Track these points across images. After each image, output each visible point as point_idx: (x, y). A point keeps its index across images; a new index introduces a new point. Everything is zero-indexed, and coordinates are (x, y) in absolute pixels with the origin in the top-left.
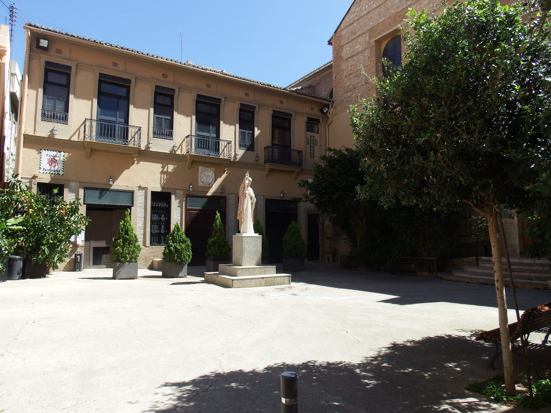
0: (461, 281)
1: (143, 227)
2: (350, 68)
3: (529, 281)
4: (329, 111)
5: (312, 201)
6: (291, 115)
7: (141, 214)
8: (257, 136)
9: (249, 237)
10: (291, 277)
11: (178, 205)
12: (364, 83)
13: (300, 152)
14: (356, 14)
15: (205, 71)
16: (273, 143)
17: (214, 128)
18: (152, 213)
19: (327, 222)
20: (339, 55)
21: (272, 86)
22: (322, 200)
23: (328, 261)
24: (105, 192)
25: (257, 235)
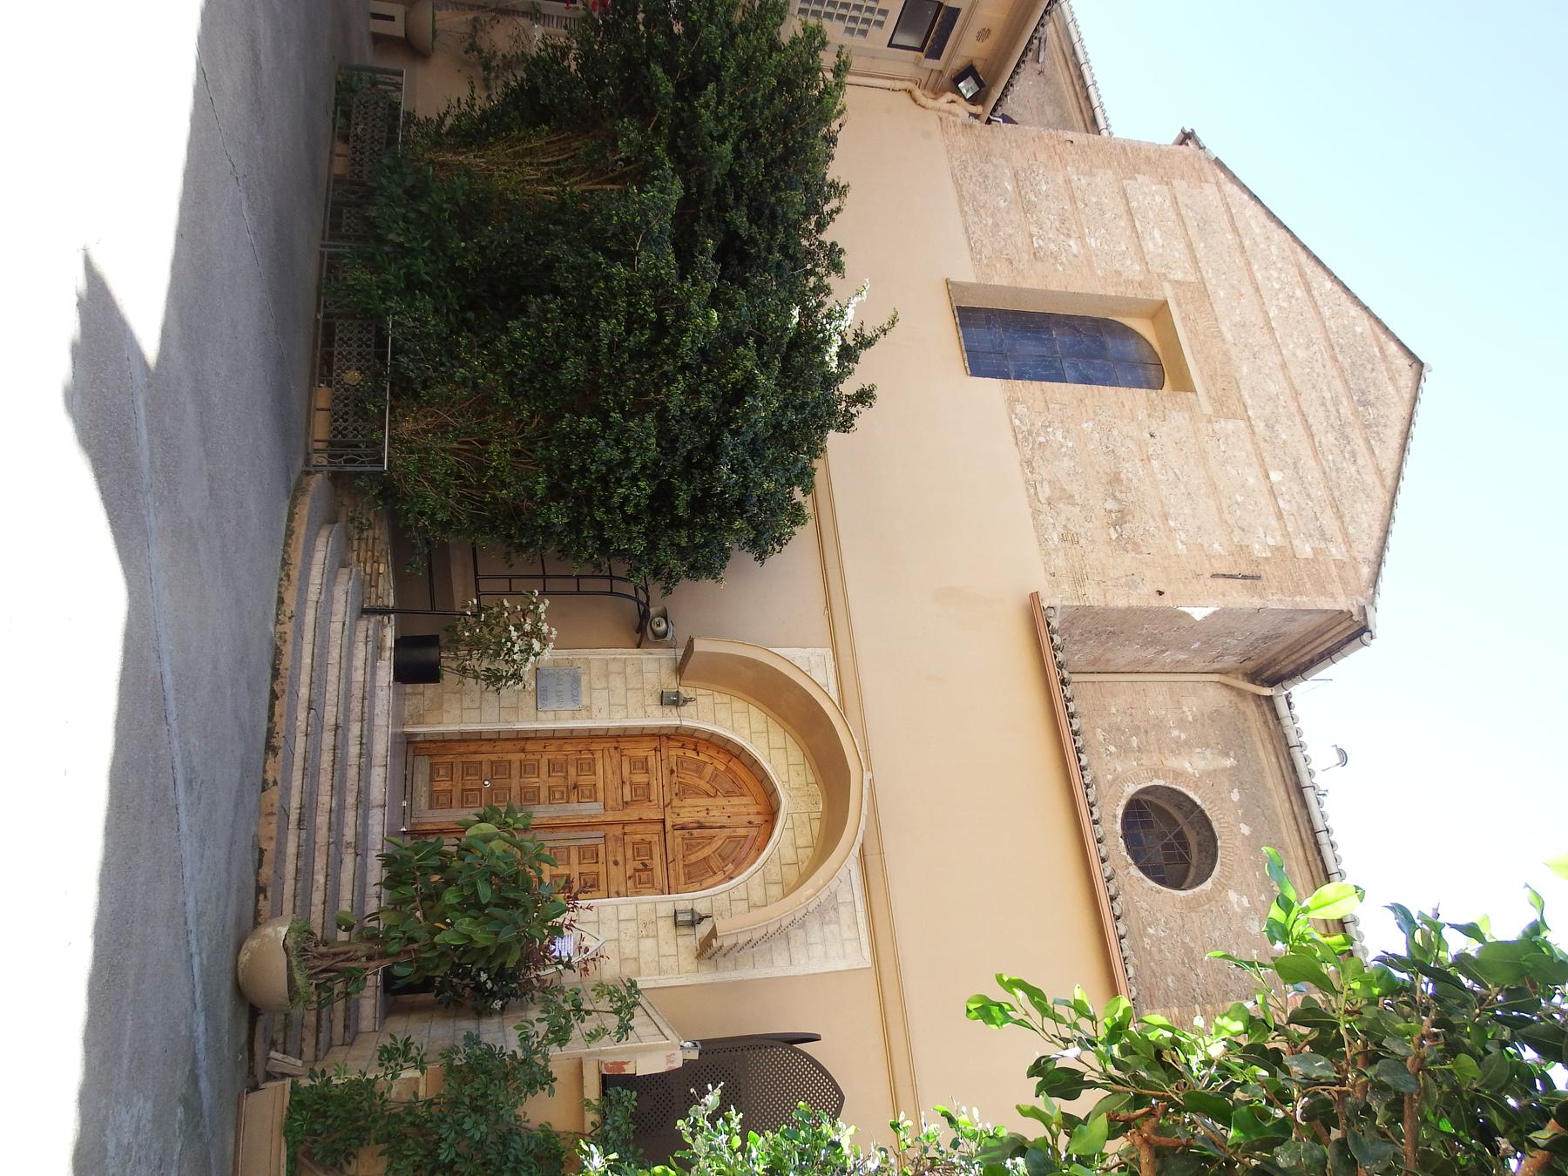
0: (288, 575)
2: (1094, 200)
3: (294, 817)
12: (1036, 245)
14: (1262, 246)
19: (538, 31)
20: (1143, 167)
22: (641, 16)
23: (376, 16)
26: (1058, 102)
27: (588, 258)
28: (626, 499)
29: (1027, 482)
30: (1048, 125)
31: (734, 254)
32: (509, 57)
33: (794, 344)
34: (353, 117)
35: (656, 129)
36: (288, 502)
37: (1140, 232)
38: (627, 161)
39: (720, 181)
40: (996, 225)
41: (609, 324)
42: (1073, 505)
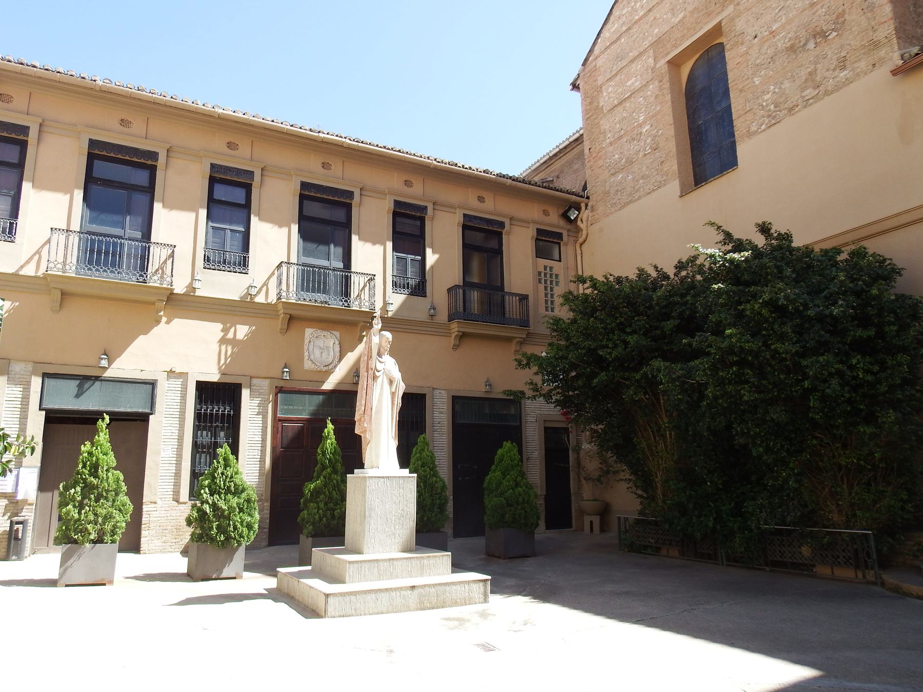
1: (175, 459)
2: (618, 125)
4: (580, 216)
5: (548, 396)
6: (502, 225)
7: (170, 431)
8: (432, 267)
9: (383, 477)
10: (489, 583)
11: (257, 411)
12: (650, 151)
13: (524, 298)
14: (624, 19)
15: (317, 134)
16: (467, 280)
17: (340, 250)
18: (197, 428)
19: (586, 446)
20: (595, 104)
21: (459, 165)
22: (571, 393)
24: (90, 383)
25: (406, 472)
26: (570, 163)
27: (705, 411)
28: (867, 371)
29: (805, 107)
30: (583, 164)
31: (691, 325)
32: (600, 461)
33: (737, 281)
34: (645, 544)
35: (626, 379)
36: (908, 599)
37: (630, 93)
38: (645, 394)
39: (649, 340)
40: (643, 177)
41: (744, 395)
42: (816, 70)
